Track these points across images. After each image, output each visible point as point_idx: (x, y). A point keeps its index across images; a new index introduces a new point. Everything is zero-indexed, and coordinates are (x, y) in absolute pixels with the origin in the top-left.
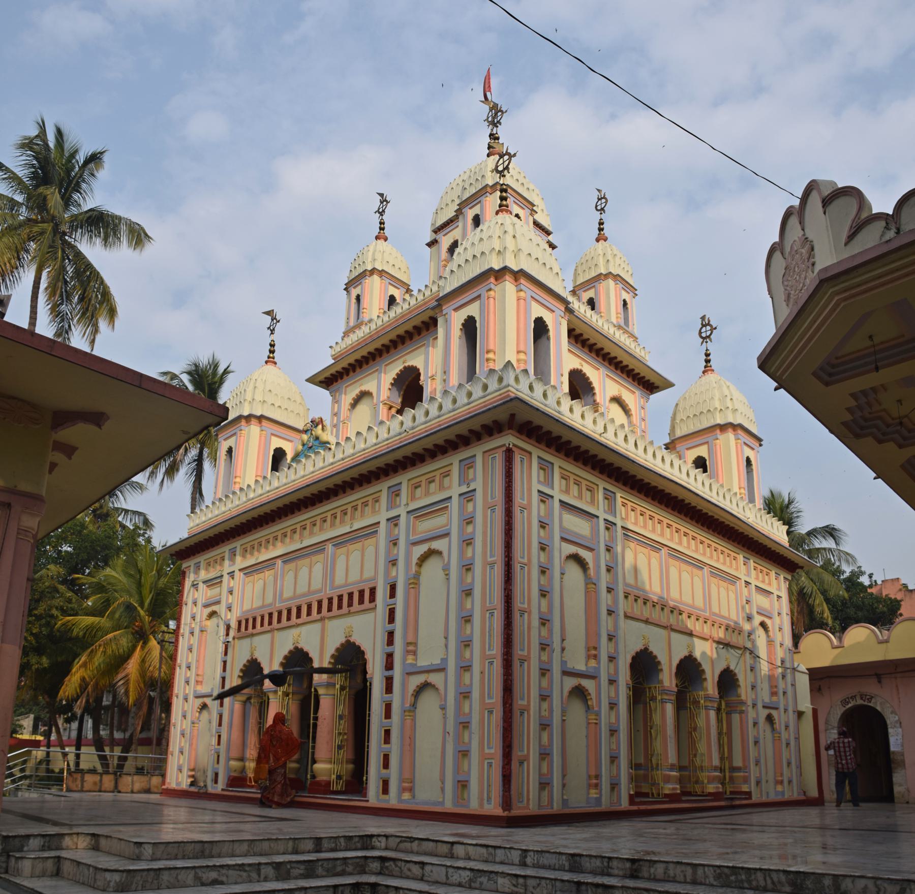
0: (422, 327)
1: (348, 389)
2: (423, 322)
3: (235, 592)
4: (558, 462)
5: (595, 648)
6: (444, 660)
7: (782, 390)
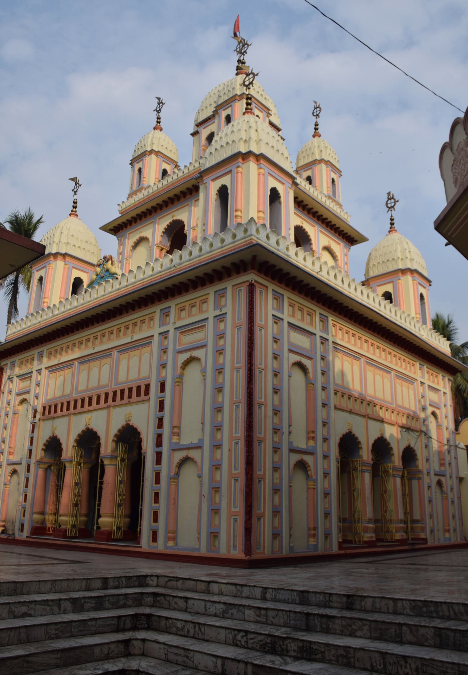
0: (187, 192)
2: (187, 189)
4: (287, 294)
5: (313, 432)
6: (201, 440)
7: (451, 246)
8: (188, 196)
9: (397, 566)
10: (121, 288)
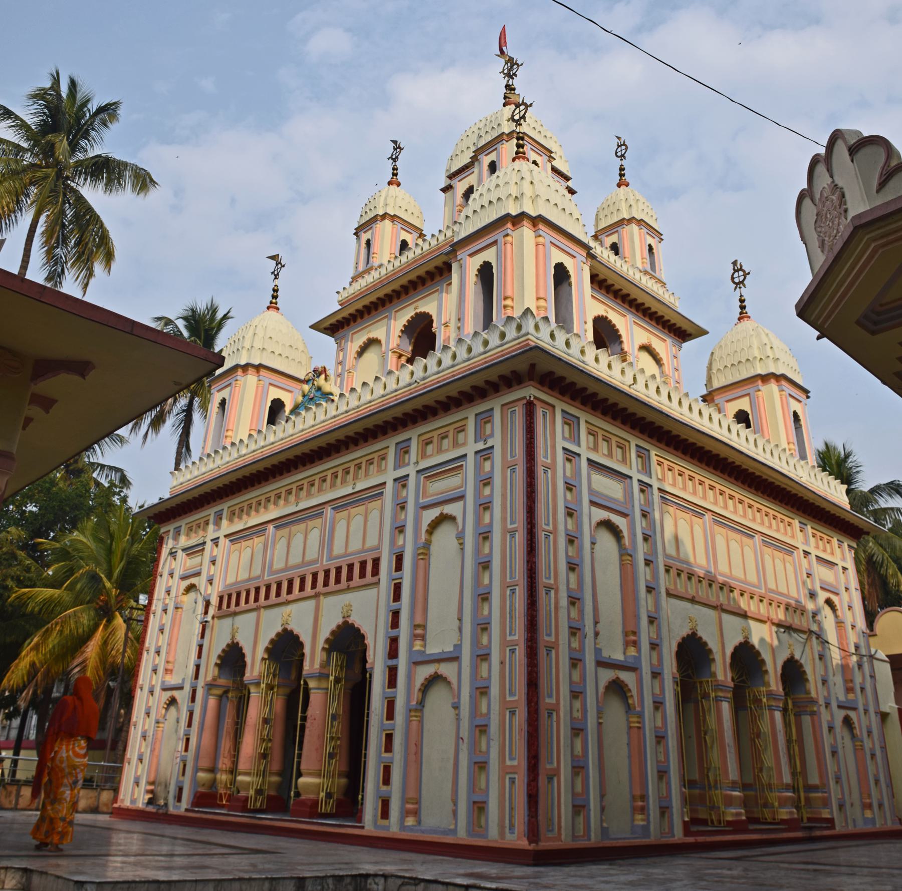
0: (435, 273)
1: (355, 336)
3: (218, 563)
4: (584, 417)
5: (634, 633)
6: (458, 647)
7: (825, 339)
8: (438, 278)
9: (782, 865)
10: (338, 416)
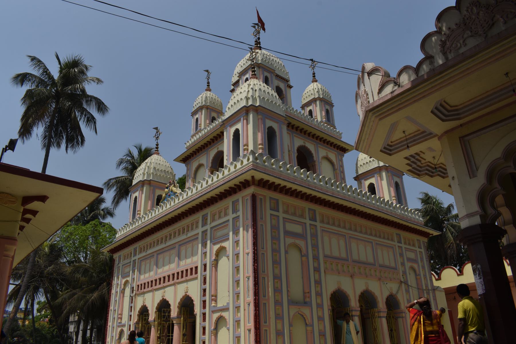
6: (228, 304)
